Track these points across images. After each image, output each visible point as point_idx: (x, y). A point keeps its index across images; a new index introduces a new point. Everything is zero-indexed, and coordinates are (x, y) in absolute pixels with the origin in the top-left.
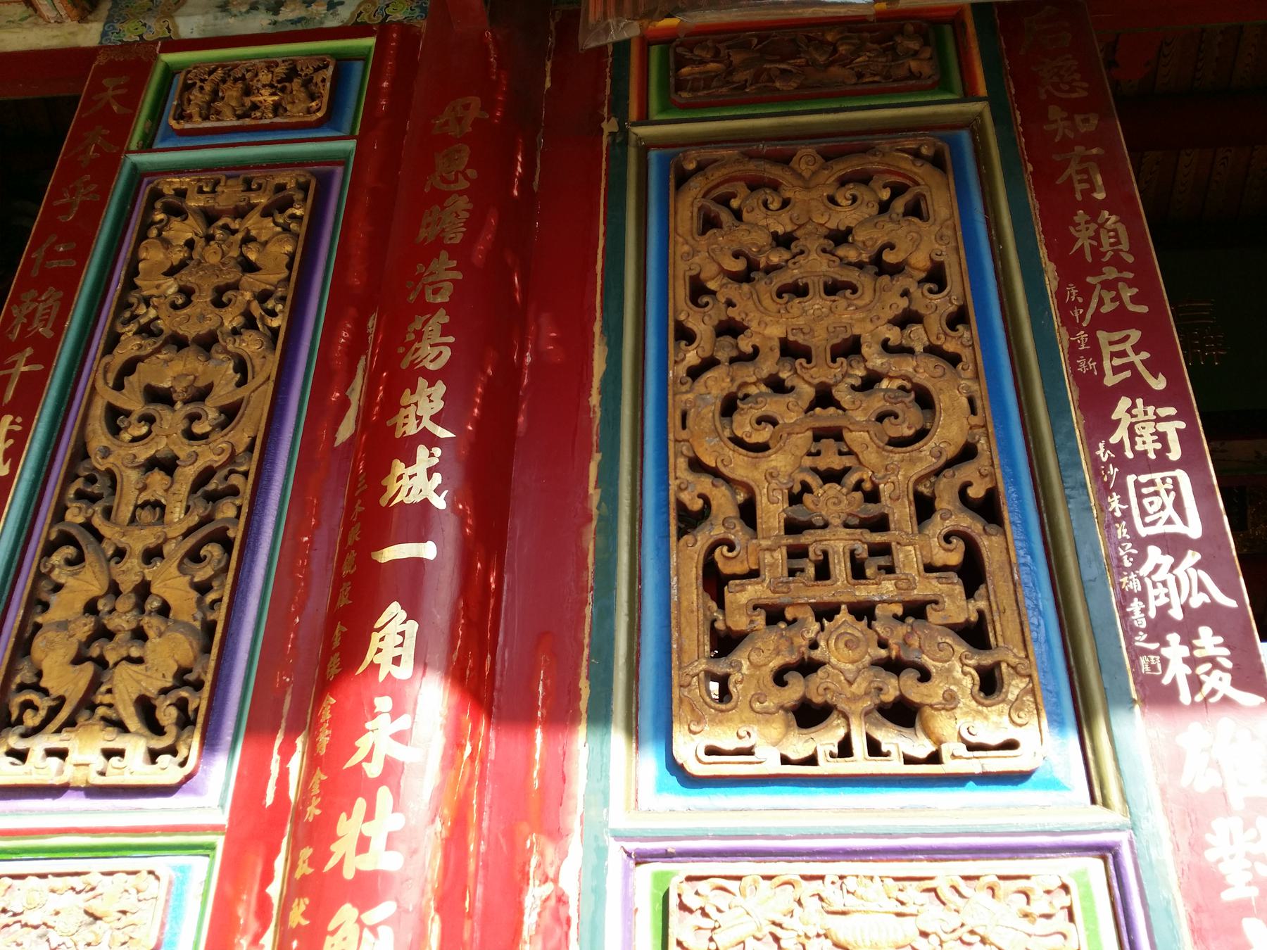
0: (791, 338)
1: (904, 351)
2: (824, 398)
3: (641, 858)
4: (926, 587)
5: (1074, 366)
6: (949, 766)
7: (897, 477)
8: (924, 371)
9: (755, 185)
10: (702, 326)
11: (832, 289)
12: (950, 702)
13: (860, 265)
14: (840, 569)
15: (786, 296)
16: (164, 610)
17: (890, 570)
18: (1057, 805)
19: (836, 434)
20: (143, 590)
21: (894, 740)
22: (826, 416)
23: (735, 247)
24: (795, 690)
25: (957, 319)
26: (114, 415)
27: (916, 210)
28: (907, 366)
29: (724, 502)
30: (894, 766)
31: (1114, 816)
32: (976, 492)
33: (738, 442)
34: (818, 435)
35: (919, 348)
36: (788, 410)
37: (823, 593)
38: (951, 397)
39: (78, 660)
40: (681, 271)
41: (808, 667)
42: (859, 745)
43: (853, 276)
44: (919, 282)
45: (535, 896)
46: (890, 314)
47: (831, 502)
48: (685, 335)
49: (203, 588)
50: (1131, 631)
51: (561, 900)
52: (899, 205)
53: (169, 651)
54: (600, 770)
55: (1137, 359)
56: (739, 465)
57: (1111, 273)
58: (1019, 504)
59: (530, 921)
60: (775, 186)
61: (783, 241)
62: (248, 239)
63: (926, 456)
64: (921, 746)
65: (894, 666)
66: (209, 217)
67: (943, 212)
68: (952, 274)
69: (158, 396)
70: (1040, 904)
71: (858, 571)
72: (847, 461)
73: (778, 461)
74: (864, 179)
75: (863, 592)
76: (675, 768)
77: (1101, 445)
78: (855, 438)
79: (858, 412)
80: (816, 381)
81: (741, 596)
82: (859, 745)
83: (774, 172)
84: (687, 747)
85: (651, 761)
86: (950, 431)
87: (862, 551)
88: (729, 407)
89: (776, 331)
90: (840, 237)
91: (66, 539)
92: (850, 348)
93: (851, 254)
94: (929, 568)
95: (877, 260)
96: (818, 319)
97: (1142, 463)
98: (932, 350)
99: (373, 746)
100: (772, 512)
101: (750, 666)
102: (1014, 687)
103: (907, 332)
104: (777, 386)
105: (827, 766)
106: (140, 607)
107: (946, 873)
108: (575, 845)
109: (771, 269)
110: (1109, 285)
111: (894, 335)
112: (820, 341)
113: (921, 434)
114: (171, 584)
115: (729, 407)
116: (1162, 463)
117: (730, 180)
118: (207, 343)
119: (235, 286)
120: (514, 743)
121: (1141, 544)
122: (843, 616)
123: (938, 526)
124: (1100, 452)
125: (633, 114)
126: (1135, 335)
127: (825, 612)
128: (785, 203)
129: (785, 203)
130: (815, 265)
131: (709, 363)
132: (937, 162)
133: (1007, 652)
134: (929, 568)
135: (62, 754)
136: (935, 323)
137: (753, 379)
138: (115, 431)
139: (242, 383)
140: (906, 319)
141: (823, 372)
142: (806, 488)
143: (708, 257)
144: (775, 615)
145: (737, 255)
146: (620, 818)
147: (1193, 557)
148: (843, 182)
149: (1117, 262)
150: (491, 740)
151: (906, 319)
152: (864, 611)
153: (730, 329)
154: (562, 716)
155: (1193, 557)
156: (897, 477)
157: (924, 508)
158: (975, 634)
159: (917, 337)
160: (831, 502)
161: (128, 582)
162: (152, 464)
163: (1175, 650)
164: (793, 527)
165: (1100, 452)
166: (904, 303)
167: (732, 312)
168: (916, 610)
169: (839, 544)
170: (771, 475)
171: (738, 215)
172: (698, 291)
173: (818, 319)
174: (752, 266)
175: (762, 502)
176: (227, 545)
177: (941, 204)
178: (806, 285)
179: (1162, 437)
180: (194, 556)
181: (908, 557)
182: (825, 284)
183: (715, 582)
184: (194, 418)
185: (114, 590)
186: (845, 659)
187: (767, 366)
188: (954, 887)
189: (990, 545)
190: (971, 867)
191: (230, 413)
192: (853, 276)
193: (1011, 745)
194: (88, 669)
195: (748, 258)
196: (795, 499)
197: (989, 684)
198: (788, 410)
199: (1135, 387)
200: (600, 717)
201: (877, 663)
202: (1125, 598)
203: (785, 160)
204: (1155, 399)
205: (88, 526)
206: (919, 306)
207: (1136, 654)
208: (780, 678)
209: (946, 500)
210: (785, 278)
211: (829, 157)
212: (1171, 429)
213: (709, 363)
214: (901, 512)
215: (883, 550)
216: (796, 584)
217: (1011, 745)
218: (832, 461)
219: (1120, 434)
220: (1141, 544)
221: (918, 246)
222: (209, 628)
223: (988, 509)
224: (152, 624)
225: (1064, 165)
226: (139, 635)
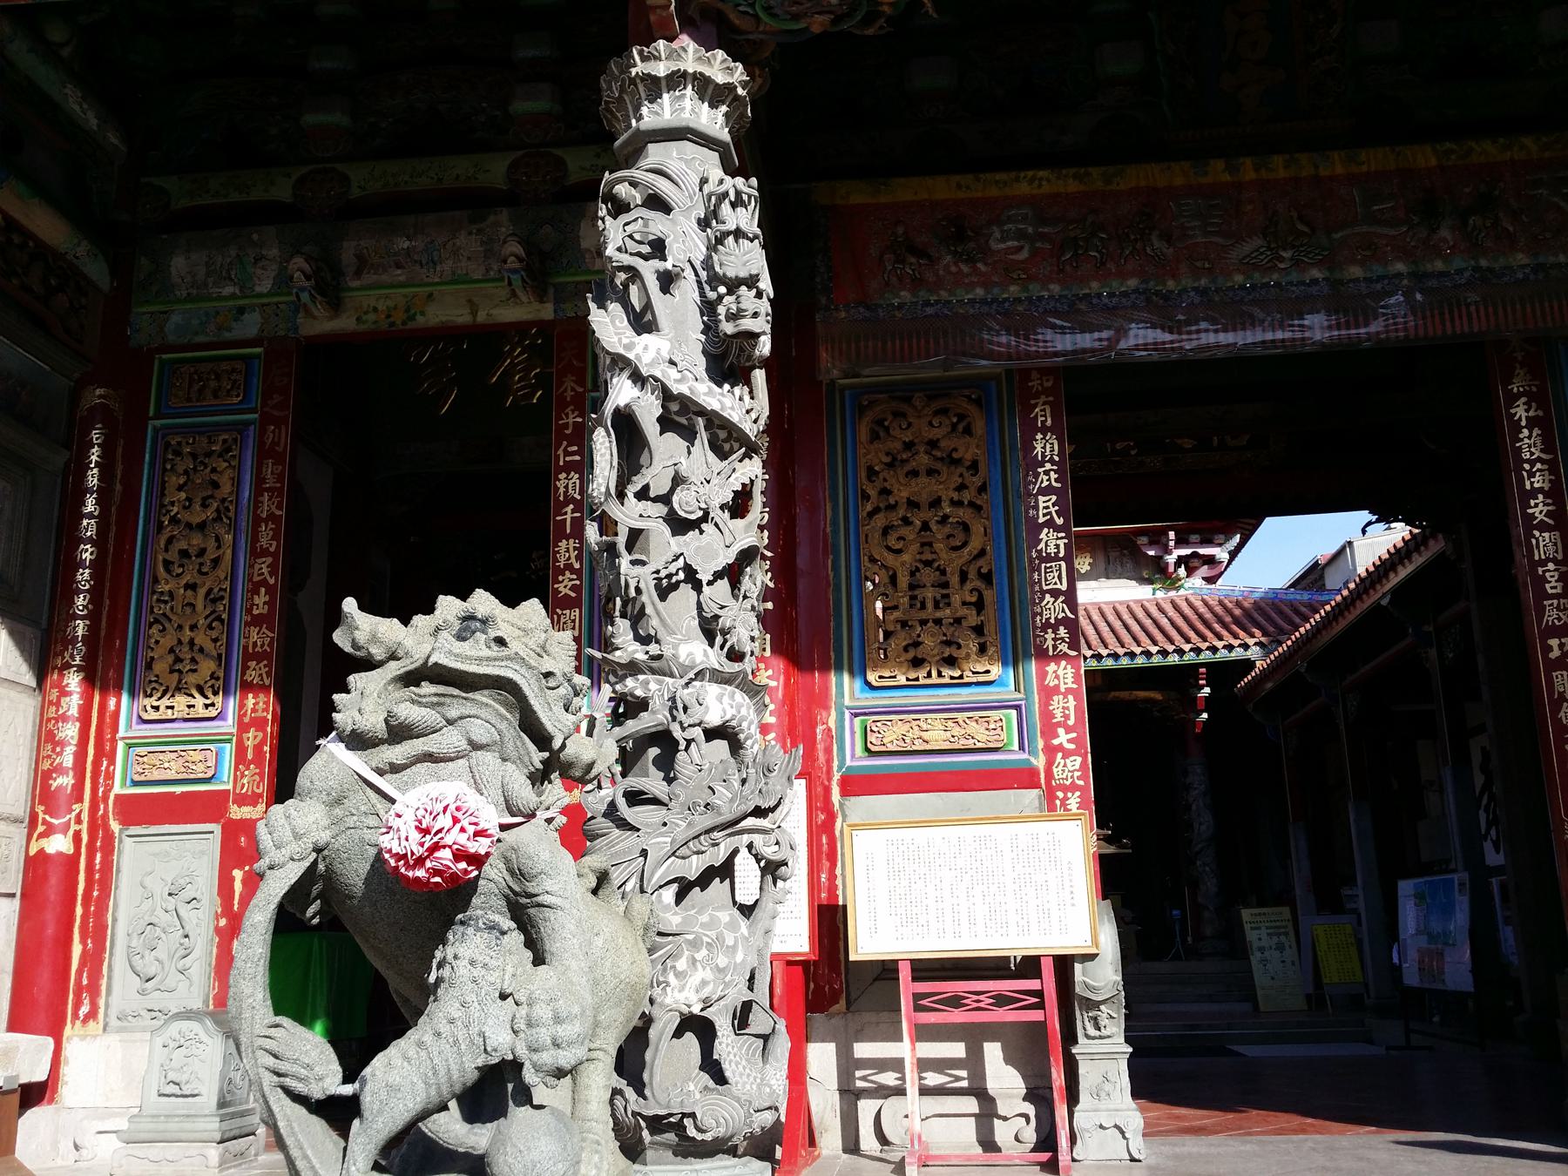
2: (925, 526)
3: (856, 715)
4: (963, 611)
6: (966, 680)
7: (954, 563)
8: (964, 514)
9: (898, 415)
10: (872, 493)
11: (931, 472)
12: (968, 656)
13: (942, 459)
14: (930, 605)
16: (201, 650)
17: (949, 605)
18: (1007, 692)
19: (930, 544)
20: (192, 643)
21: (947, 672)
24: (911, 655)
25: (982, 489)
26: (167, 564)
27: (968, 431)
28: (961, 512)
30: (947, 680)
31: (1021, 696)
32: (984, 570)
33: (889, 548)
34: (923, 545)
37: (923, 615)
38: (977, 528)
39: (172, 672)
40: (863, 462)
42: (934, 673)
43: (938, 466)
45: (819, 729)
46: (953, 486)
47: (928, 576)
48: (866, 497)
49: (215, 641)
50: (1035, 628)
51: (829, 730)
52: (961, 427)
53: (207, 667)
54: (840, 685)
55: (1053, 510)
56: (890, 559)
57: (1048, 466)
58: (1001, 579)
59: (819, 737)
60: (904, 415)
61: (909, 446)
62: (214, 470)
64: (957, 673)
65: (948, 643)
66: (194, 456)
67: (980, 432)
68: (982, 466)
69: (184, 554)
70: (992, 726)
71: (937, 606)
73: (906, 557)
74: (943, 412)
75: (939, 614)
76: (868, 683)
78: (938, 546)
79: (939, 532)
82: (934, 673)
84: (872, 677)
85: (858, 683)
86: (975, 544)
87: (938, 597)
88: (886, 531)
89: (905, 494)
90: (933, 444)
91: (157, 621)
92: (936, 503)
94: (964, 603)
95: (950, 456)
96: (924, 488)
97: (1049, 558)
98: (972, 504)
100: (904, 581)
101: (896, 644)
102: (991, 650)
104: (906, 521)
105: (922, 682)
106: (191, 649)
107: (960, 716)
108: (833, 713)
109: (903, 461)
110: (1047, 473)
111: (956, 496)
112: (924, 498)
113: (965, 544)
114: (201, 639)
115: (886, 531)
116: (1056, 558)
118: (202, 526)
119: (211, 497)
120: (807, 678)
121: (1043, 593)
122: (930, 624)
123: (969, 586)
125: (589, 385)
126: (1054, 498)
127: (923, 623)
128: (910, 425)
129: (910, 425)
130: (923, 460)
131: (876, 510)
132: (978, 402)
133: (990, 637)
134: (964, 603)
135: (172, 708)
136: (973, 490)
138: (168, 571)
139: (219, 547)
140: (961, 488)
141: (926, 514)
142: (918, 569)
143: (876, 456)
144: (904, 624)
145: (887, 454)
146: (847, 702)
147: (1062, 598)
148: (936, 413)
149: (1052, 461)
150: (798, 678)
151: (961, 488)
152: (938, 622)
153: (885, 492)
154: (825, 668)
155: (1062, 598)
156: (954, 563)
157: (964, 577)
158: (979, 630)
159: (966, 496)
160: (928, 576)
161: (186, 640)
162: (187, 587)
163: (1050, 635)
164: (912, 587)
167: (886, 485)
168: (958, 621)
169: (929, 594)
170: (903, 564)
171: (887, 429)
172: (872, 473)
175: (899, 575)
176: (222, 621)
177: (979, 426)
179: (1057, 546)
181: (956, 599)
184: (201, 564)
185: (180, 642)
186: (930, 642)
187: (901, 513)
189: (988, 595)
190: (970, 714)
191: (216, 562)
192: (938, 466)
193: (988, 672)
194: (176, 675)
196: (912, 574)
197: (982, 650)
199: (1050, 524)
200: (839, 669)
201: (943, 642)
202: (1035, 615)
203: (908, 400)
204: (1057, 529)
205: (164, 614)
207: (1036, 636)
208: (906, 649)
209: (972, 575)
210: (908, 468)
211: (931, 398)
212: (1061, 543)
213: (876, 510)
214: (955, 580)
215: (946, 596)
216: (913, 611)
217: (988, 672)
219: (1042, 545)
220: (1043, 593)
221: (969, 450)
222: (220, 656)
223: (987, 578)
224: (198, 657)
225: (1035, 406)
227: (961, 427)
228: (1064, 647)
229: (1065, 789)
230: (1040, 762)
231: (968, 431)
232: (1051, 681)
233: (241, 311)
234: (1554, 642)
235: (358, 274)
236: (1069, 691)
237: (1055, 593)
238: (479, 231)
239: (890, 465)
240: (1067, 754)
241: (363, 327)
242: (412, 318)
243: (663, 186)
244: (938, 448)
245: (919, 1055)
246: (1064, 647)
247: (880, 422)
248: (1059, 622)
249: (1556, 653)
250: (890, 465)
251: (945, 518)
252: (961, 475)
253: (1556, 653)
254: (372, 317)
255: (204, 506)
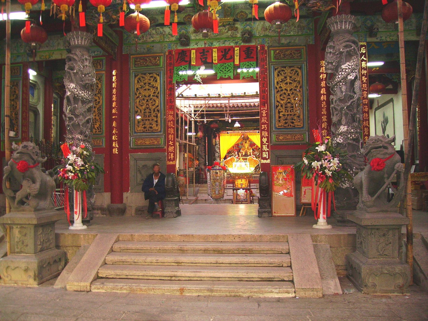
2: (289, 95)
11: (149, 90)
14: (147, 116)
22: (289, 97)
29: (139, 111)
36: (144, 102)
41: (145, 124)
43: (150, 88)
48: (276, 88)
61: (145, 84)
63: (154, 107)
65: (151, 124)
71: (291, 111)
81: (281, 114)
86: (157, 104)
88: (280, 96)
92: (149, 96)
93: (150, 85)
98: (156, 96)
100: (143, 112)
112: (147, 95)
115: (280, 96)
121: (169, 114)
127: (146, 120)
130: (147, 87)
148: (291, 70)
152: (149, 120)
153: (280, 87)
160: (289, 105)
163: (169, 123)
164: (144, 113)
168: (153, 120)
169: (147, 114)
172: (137, 89)
173: (147, 93)
180: (99, 116)
181: (152, 116)
183: (279, 112)
192: (150, 88)
196: (286, 105)
198: (144, 102)
209: (156, 110)
214: (152, 112)
218: (147, 107)
220: (169, 114)
223: (158, 111)
226: (96, 122)
228: (172, 125)
229: (170, 152)
230: (166, 148)
232: (169, 132)
233: (18, 56)
234: (263, 126)
235: (39, 48)
236: (172, 134)
237: (171, 115)
238: (62, 39)
239: (281, 82)
240: (171, 146)
241: (41, 60)
242: (50, 57)
243: (75, 57)
246: (172, 125)
247: (139, 79)
248: (171, 120)
249: (263, 128)
250: (281, 82)
251: (151, 99)
253: (263, 128)
254: (42, 57)
255: (13, 96)
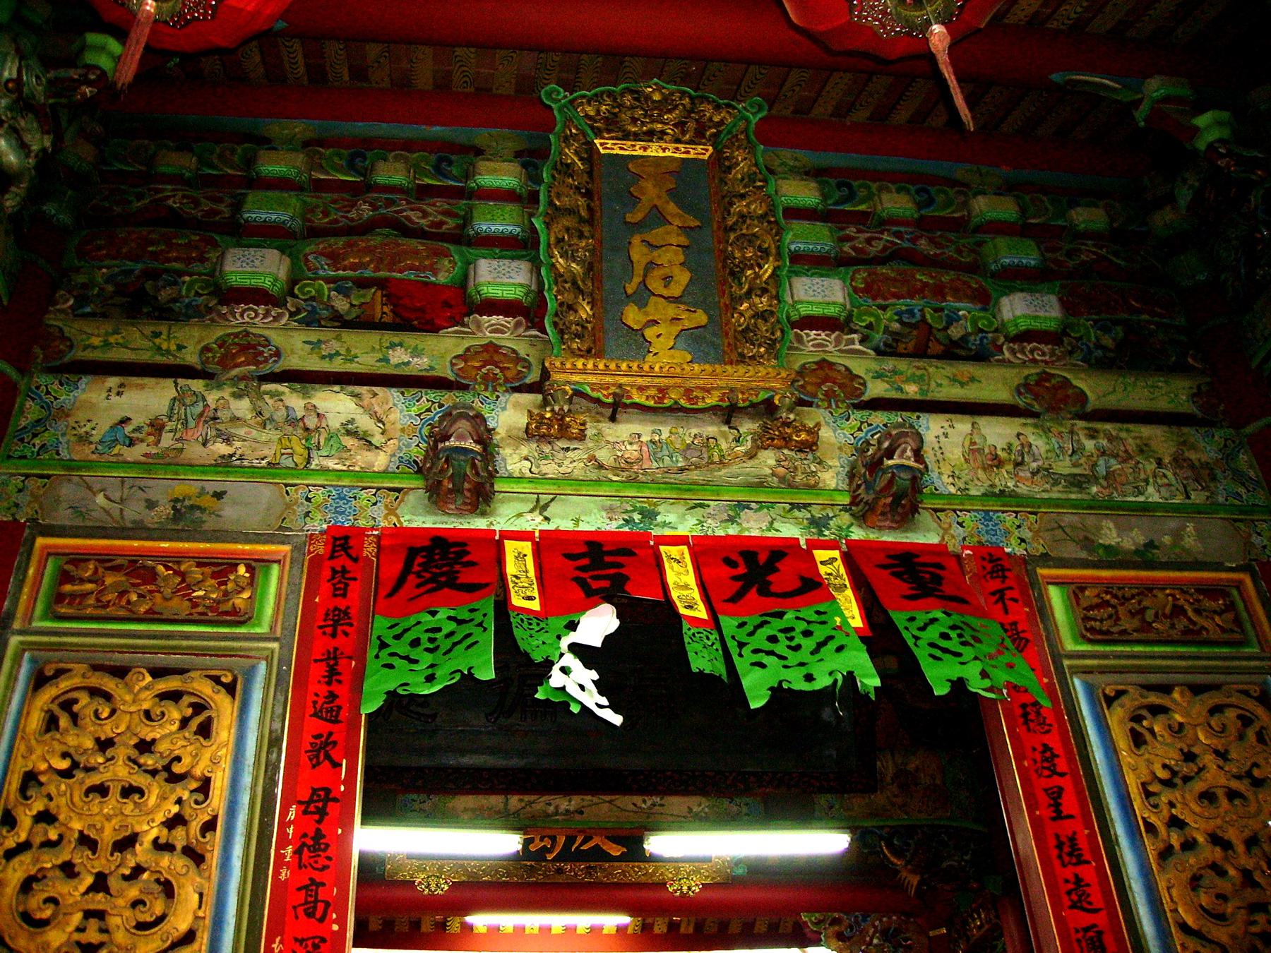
0: (86, 832)
1: (169, 847)
5: (277, 873)
11: (129, 791)
13: (153, 773)
15: (91, 796)
22: (98, 901)
23: (64, 749)
25: (210, 826)
34: (88, 914)
35: (179, 847)
43: (140, 780)
44: (191, 792)
52: (194, 724)
72: (104, 937)
77: (278, 939)
78: (114, 921)
80: (95, 871)
83: (109, 684)
89: (77, 825)
92: (127, 843)
95: (167, 768)
98: (189, 851)
99: (878, 566)
103: (174, 832)
104: (69, 870)
109: (88, 770)
117: (77, 689)
124: (275, 946)
137: (49, 865)
159: (179, 837)
165: (275, 946)
166: (175, 809)
174: (75, 765)
178: (108, 788)
182: (123, 788)
188: (825, 613)
195: (73, 760)
206: (187, 813)
210: (95, 779)
227: (194, 724)
231: (205, 731)
244: (192, 705)
245: (511, 547)
247: (67, 705)
252: (179, 801)
